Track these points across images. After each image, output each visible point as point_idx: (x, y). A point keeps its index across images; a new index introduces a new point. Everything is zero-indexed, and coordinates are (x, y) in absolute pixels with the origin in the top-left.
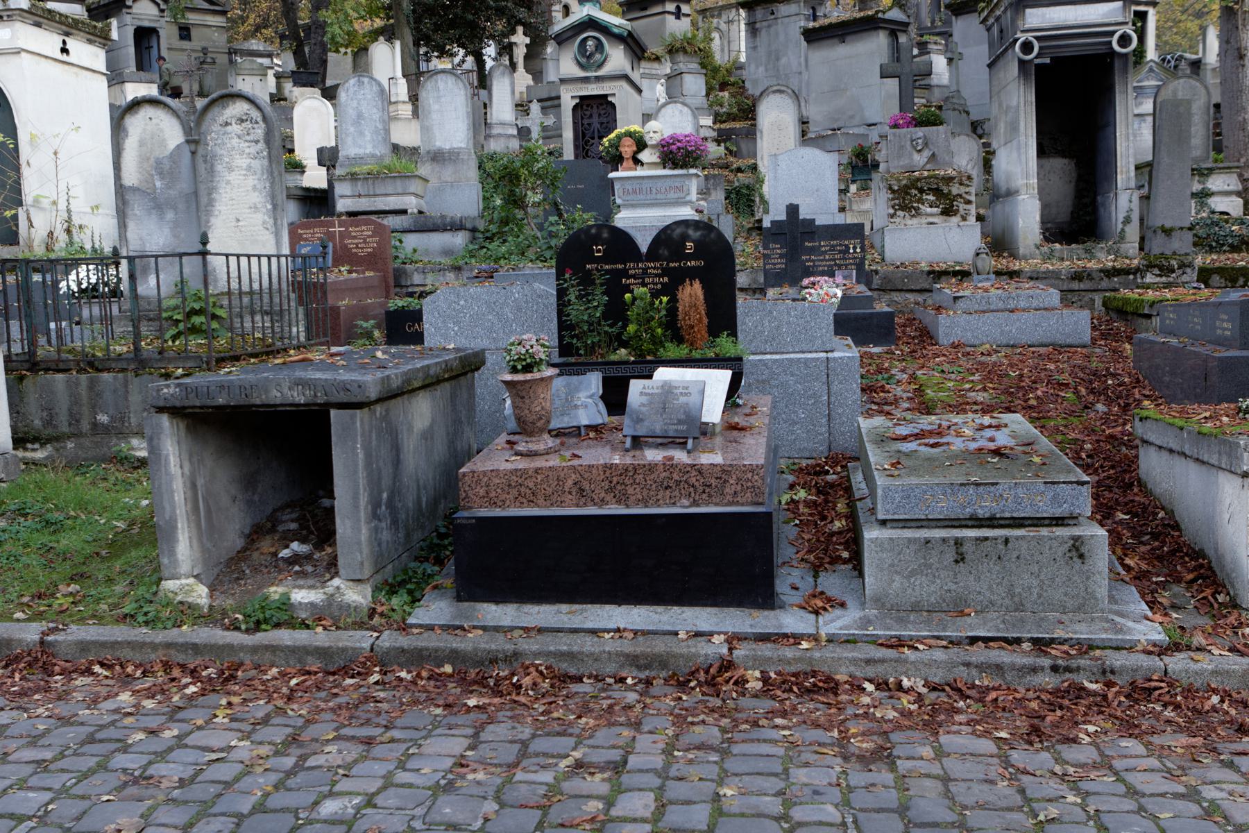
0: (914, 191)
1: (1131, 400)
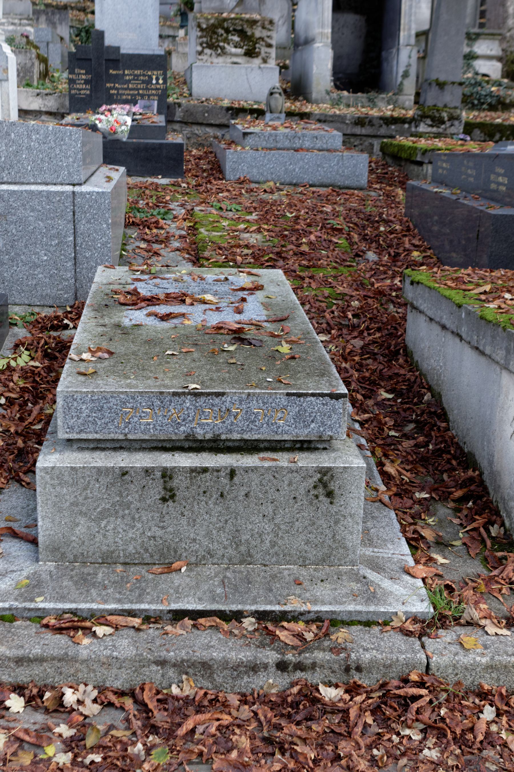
0: (221, 31)
1: (401, 250)
